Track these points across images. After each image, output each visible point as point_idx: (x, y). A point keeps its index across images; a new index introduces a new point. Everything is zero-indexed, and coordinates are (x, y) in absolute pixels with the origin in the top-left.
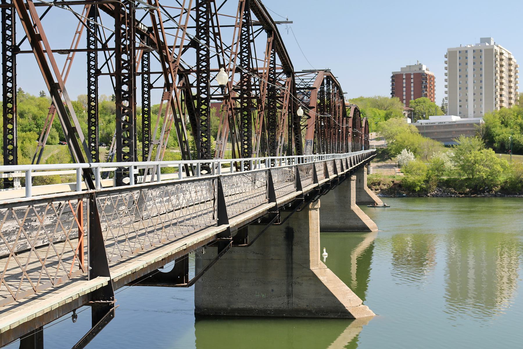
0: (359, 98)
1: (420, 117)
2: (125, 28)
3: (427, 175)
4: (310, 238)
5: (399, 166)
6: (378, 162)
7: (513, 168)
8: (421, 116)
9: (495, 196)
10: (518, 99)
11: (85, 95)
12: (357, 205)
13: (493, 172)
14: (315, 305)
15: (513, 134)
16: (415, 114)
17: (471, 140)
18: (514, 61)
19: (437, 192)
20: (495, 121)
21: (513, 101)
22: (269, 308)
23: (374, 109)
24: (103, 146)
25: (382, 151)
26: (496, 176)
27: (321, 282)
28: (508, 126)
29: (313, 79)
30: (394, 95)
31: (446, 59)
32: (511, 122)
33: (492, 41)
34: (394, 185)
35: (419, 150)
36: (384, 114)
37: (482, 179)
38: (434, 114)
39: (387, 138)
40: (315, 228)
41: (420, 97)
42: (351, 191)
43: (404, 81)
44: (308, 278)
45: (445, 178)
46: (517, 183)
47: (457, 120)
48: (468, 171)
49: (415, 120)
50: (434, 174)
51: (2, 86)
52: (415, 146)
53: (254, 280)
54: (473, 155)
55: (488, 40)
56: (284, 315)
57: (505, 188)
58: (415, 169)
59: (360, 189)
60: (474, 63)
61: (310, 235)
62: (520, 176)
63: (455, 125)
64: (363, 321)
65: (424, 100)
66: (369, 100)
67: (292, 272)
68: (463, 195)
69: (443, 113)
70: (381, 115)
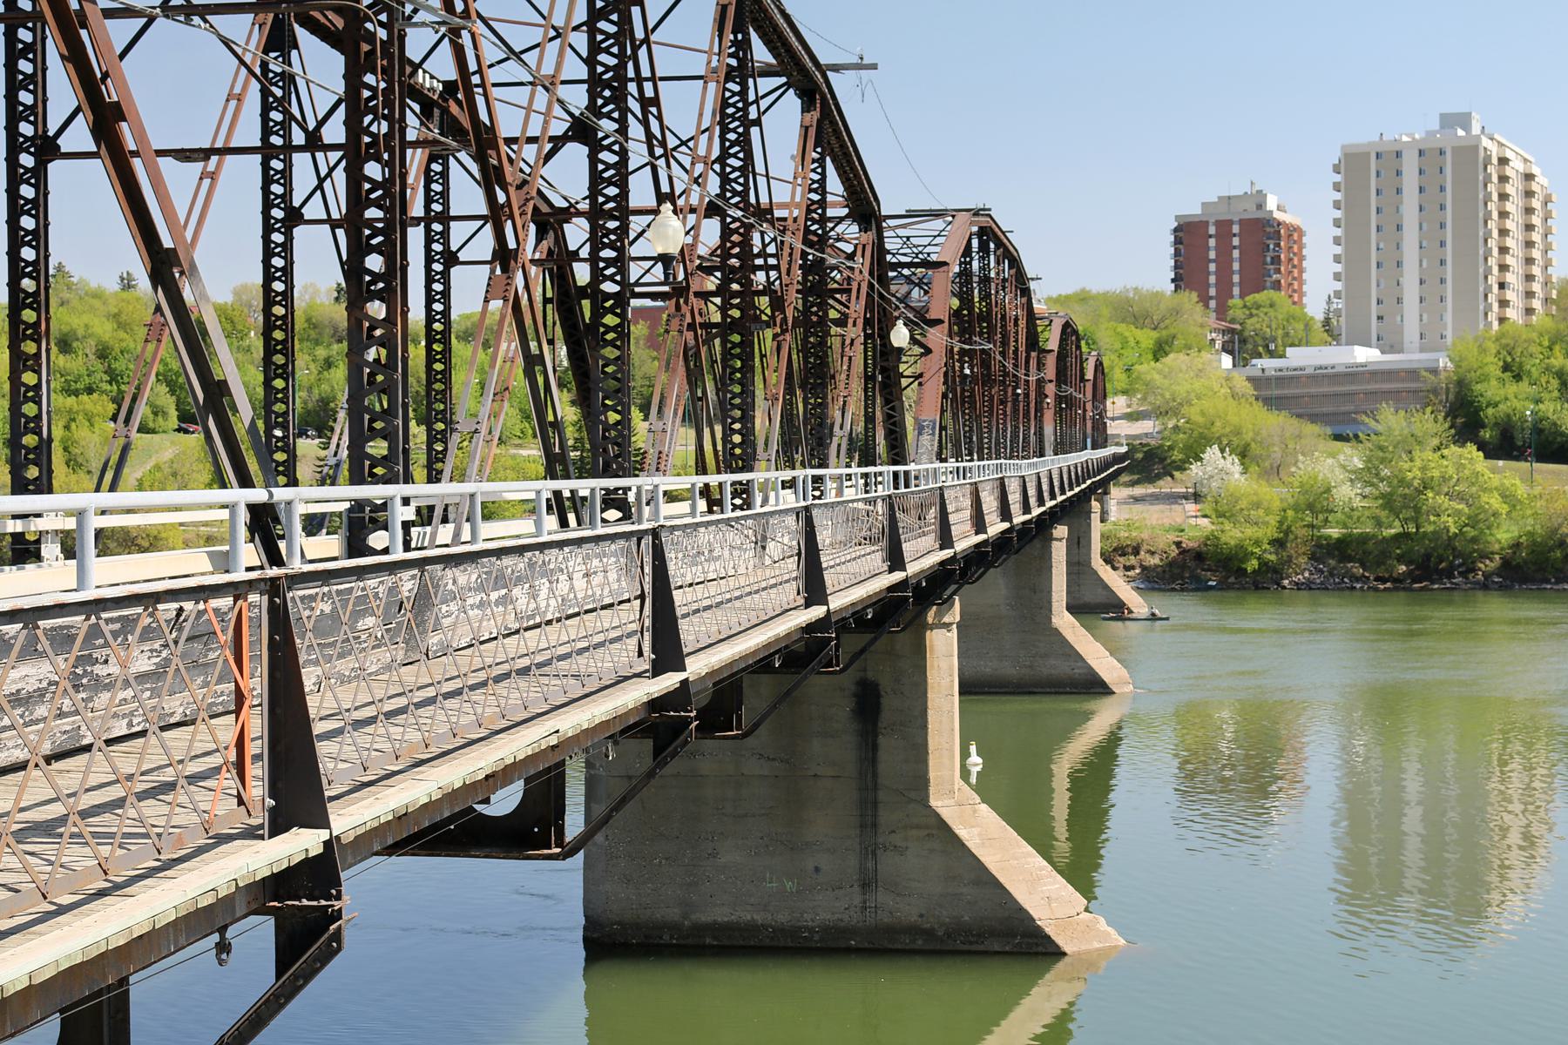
0: (1076, 294)
1: (1261, 349)
2: (375, 84)
3: (1281, 523)
4: (929, 711)
5: (1197, 497)
6: (1133, 484)
7: (1538, 504)
8: (1264, 347)
9: (1485, 586)
10: (1554, 297)
11: (254, 285)
12: (1071, 613)
13: (1477, 515)
14: (944, 913)
15: (1538, 401)
16: (1243, 341)
17: (1413, 420)
18: (1541, 182)
19: (1311, 574)
20: (1485, 361)
21: (1537, 304)
22: (806, 921)
23: (1122, 328)
24: (308, 436)
25: (1145, 452)
26: (1488, 528)
27: (963, 845)
28: (1524, 377)
29: (939, 235)
30: (1182, 284)
31: (1338, 178)
32: (1533, 366)
33: (1474, 122)
34: (1180, 553)
35: (1255, 449)
36: (1151, 342)
37: (1445, 537)
38: (1300, 340)
39: (1159, 413)
40: (945, 682)
41: (1258, 292)
42: (1054, 572)
43: (1212, 242)
44: (924, 832)
45: (1334, 532)
46: (1551, 549)
47: (1370, 360)
48: (1404, 511)
49: (1245, 359)
50: (1303, 520)
51: (6, 258)
52: (1245, 436)
53: (762, 838)
54: (1418, 463)
55: (1464, 120)
56: (853, 943)
57: (1514, 563)
58: (1243, 507)
59: (1078, 567)
60: (1421, 188)
61: (930, 704)
62: (1560, 526)
63: (1363, 373)
64: (1089, 962)
65: (1271, 299)
66: (1106, 298)
67: (875, 816)
68: (1388, 585)
69: (1329, 339)
70: (1143, 346)
